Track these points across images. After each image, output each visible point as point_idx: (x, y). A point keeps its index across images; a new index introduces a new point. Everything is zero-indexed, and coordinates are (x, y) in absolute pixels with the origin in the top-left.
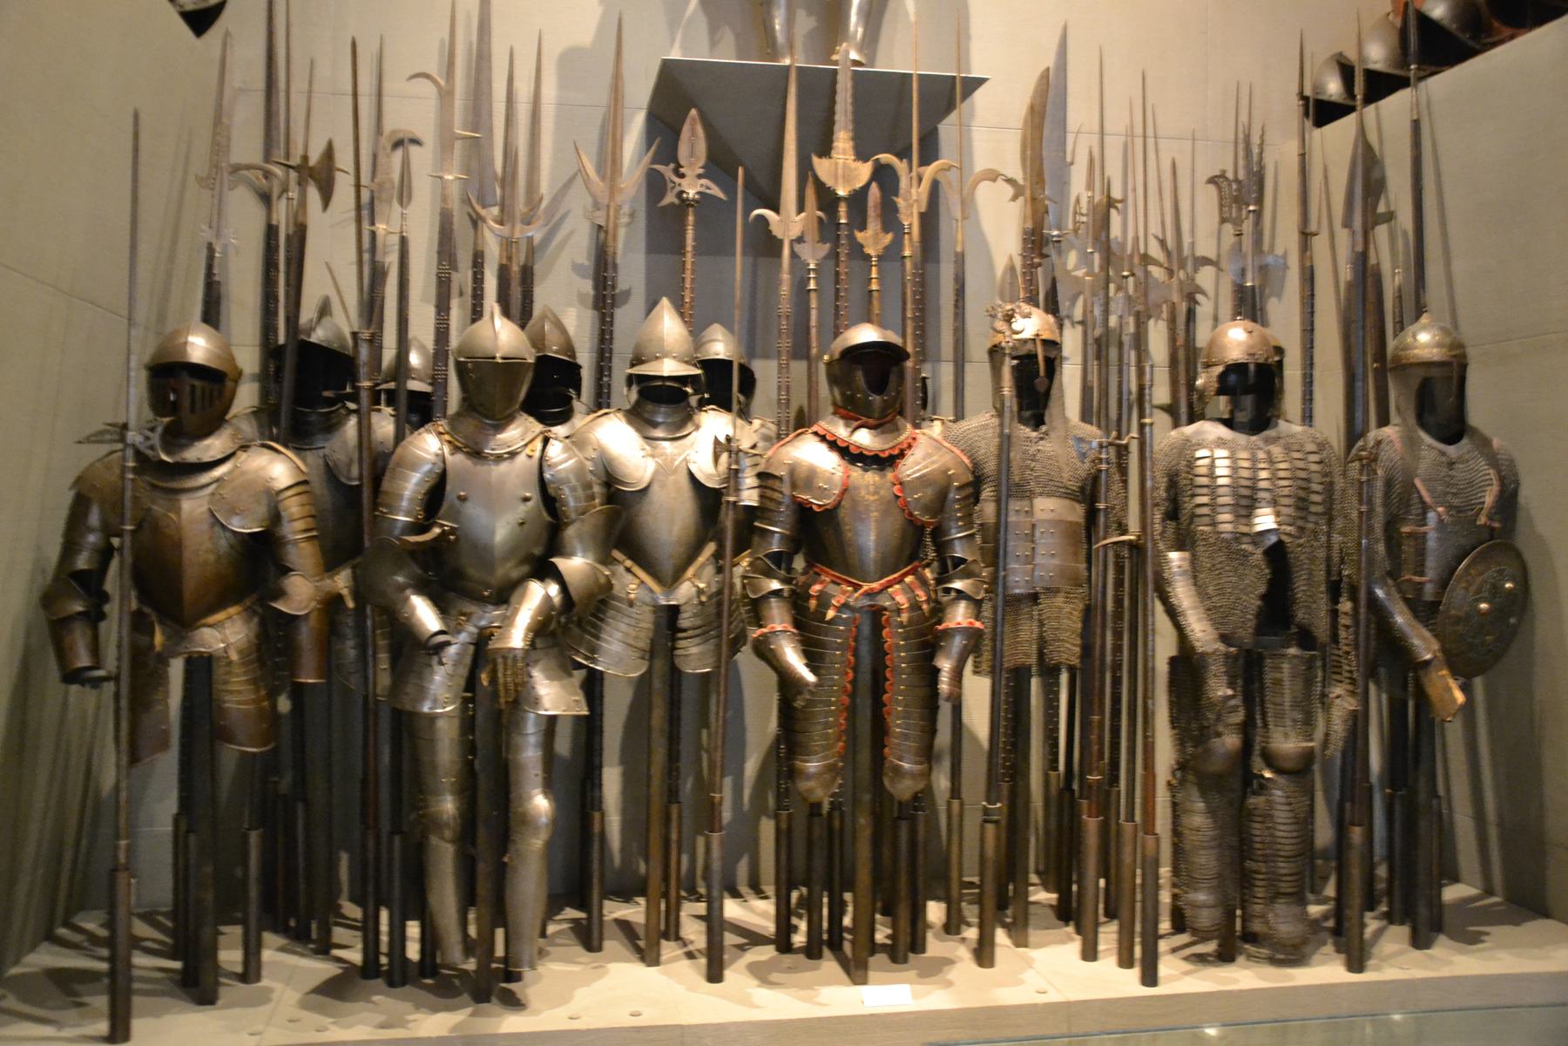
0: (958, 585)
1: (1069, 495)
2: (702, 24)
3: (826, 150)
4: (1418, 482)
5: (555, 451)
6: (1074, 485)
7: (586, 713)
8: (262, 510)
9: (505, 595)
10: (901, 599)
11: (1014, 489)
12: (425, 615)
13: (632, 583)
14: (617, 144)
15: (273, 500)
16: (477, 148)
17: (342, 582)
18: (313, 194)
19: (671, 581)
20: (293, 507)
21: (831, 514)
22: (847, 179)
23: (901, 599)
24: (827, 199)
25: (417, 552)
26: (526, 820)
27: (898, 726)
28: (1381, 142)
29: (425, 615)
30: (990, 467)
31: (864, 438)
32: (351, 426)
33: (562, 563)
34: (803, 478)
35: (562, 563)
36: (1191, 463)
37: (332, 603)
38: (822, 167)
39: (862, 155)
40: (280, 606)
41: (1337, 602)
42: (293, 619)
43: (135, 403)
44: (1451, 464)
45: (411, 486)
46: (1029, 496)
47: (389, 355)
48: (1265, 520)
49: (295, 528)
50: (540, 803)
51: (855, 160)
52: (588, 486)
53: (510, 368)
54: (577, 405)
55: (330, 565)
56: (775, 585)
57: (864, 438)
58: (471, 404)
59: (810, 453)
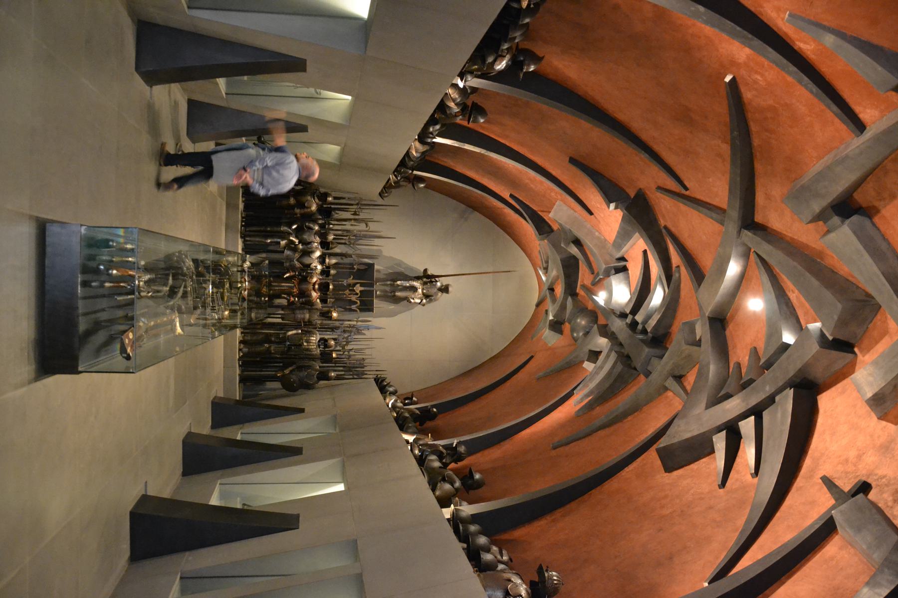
0: (296, 299)
1: (309, 319)
2: (387, 272)
3: (361, 286)
4: (310, 370)
5: (316, 244)
6: (311, 320)
8: (309, 206)
9: (297, 237)
11: (310, 311)
12: (294, 227)
13: (297, 255)
14: (366, 258)
15: (310, 208)
16: (365, 237)
17: (298, 215)
18: (353, 213)
19: (298, 260)
20: (309, 210)
21: (307, 281)
22: (357, 289)
24: (355, 285)
26: (267, 239)
28: (352, 345)
29: (294, 227)
30: (314, 307)
31: (317, 287)
32: (321, 217)
33: (300, 245)
35: (300, 245)
36: (313, 334)
37: (296, 214)
38: (358, 285)
39: (360, 291)
40: (296, 208)
42: (294, 209)
43: (322, 190)
46: (309, 313)
47: (333, 222)
48: (305, 344)
49: (306, 210)
50: (269, 241)
52: (311, 248)
53: (326, 239)
54: (323, 250)
55: (301, 214)
56: (297, 273)
57: (317, 287)
58: (322, 233)
59: (315, 280)
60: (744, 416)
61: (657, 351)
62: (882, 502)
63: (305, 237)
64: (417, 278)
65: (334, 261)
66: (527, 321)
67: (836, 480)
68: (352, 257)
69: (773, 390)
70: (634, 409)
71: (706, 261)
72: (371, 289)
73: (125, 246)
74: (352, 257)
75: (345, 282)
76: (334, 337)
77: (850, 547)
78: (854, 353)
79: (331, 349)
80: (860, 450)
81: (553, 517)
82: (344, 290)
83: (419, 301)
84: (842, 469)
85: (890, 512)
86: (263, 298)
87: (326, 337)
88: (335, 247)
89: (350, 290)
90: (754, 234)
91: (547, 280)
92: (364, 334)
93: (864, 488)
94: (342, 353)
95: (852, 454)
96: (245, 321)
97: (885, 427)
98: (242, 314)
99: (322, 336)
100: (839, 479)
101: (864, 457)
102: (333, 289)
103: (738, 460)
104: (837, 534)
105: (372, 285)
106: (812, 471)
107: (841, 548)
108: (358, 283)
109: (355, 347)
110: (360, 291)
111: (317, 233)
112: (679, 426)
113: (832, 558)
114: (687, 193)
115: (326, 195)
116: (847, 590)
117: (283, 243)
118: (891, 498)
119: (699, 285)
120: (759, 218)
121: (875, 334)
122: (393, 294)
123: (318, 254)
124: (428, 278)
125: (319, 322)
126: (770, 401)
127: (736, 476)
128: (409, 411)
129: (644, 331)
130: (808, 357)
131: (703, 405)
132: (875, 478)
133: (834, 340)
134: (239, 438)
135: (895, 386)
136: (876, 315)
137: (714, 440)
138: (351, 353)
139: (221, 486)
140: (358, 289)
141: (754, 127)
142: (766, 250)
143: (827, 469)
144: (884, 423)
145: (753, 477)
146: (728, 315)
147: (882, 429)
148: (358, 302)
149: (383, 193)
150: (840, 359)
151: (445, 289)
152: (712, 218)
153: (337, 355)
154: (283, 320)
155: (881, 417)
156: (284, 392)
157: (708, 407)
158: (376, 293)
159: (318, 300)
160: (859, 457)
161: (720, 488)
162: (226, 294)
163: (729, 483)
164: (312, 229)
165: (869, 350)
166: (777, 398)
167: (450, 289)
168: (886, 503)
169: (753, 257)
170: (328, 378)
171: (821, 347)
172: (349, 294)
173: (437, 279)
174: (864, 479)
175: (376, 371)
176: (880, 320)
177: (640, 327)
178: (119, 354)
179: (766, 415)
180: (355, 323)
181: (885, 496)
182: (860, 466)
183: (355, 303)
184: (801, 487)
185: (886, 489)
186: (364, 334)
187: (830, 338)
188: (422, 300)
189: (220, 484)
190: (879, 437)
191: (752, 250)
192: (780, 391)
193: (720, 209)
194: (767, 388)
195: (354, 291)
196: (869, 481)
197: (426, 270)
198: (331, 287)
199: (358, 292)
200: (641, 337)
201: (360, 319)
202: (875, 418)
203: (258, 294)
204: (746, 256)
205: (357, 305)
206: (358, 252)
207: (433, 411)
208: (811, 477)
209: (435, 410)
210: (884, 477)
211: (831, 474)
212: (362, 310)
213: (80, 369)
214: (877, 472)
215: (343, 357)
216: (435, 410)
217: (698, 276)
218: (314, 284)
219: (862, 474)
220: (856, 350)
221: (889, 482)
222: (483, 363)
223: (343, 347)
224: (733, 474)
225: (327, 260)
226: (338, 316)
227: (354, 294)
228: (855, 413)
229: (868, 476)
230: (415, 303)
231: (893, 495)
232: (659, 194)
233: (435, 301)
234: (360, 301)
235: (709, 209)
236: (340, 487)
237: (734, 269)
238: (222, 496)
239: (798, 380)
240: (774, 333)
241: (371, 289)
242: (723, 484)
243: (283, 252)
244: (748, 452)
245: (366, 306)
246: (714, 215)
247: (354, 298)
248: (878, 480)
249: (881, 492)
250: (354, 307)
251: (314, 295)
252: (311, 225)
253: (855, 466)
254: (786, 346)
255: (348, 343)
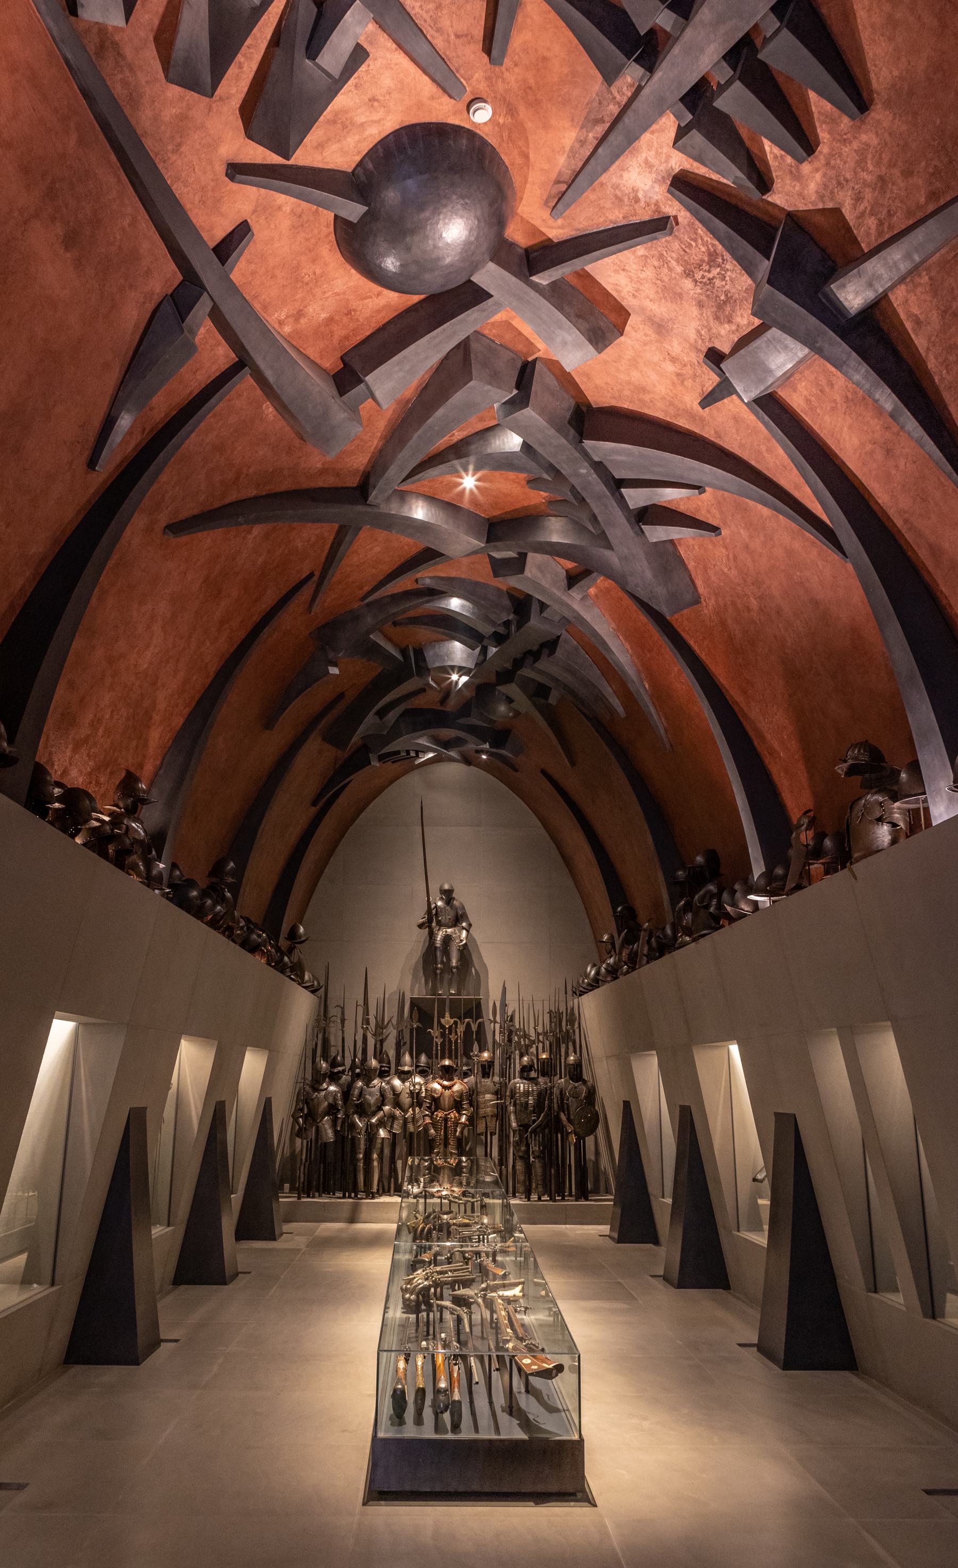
1: (493, 1094)
3: (444, 1017)
5: (383, 1084)
7: (655, 1061)
10: (453, 1116)
21: (439, 1098)
23: (453, 1116)
24: (443, 1027)
25: (357, 1105)
27: (413, 1161)
31: (446, 1083)
34: (434, 1090)
38: (442, 1021)
39: (451, 1018)
41: (424, 1261)
44: (576, 1088)
45: (356, 1092)
51: (285, 938)
57: (446, 1083)
59: (436, 1086)
60: (622, 501)
61: (535, 608)
62: (731, 336)
63: (372, 1099)
64: (432, 935)
65: (407, 1058)
66: (491, 777)
67: (705, 389)
68: (402, 1030)
69: (586, 464)
70: (629, 1112)
71: (408, 545)
72: (448, 1002)
73: (402, 1370)
74: (402, 1030)
75: (437, 1040)
76: (517, 1057)
77: (792, 379)
78: (535, 360)
79: (535, 1061)
80: (665, 358)
81: (766, 753)
82: (450, 1041)
83: (464, 933)
84: (690, 380)
85: (744, 328)
86: (464, 1164)
87: (518, 1068)
88: (387, 1056)
89: (450, 1033)
90: (374, 487)
91: (433, 750)
92: (514, 1011)
93: (715, 357)
94: (541, 1045)
95: (670, 368)
96: (497, 1192)
97: (633, 328)
98: (486, 1195)
99: (517, 1074)
100: (703, 386)
101: (674, 354)
102: (450, 1058)
103: (682, 508)
104: (776, 393)
105: (442, 1002)
106: (692, 417)
107: (795, 390)
108: (439, 1022)
109: (532, 1025)
110: (451, 1018)
111: (368, 1082)
112: (637, 585)
113: (808, 401)
114: (317, 574)
115: (316, 1070)
116: (847, 386)
117: (382, 1133)
118: (726, 326)
119: (443, 555)
120: (353, 482)
121: (508, 336)
122: (454, 970)
123: (397, 1082)
124: (431, 919)
125: (496, 1079)
126: (599, 467)
127: (703, 512)
128: (622, 947)
129: (507, 624)
130: (541, 421)
131: (607, 553)
132: (700, 342)
133: (517, 387)
134: (669, 1201)
135: (579, 316)
136: (483, 335)
137: (655, 540)
138: (540, 1030)
139: (741, 1228)
140: (448, 1020)
141: (232, 497)
142: (394, 473)
143: (691, 400)
144: (627, 328)
145: (704, 491)
146: (483, 515)
147: (636, 332)
148: (467, 1020)
149: (312, 986)
150: (542, 381)
151: (448, 895)
152: (351, 543)
153: (544, 1051)
154: (495, 1134)
155: (619, 332)
156: (600, 1131)
157: (609, 547)
158: (452, 994)
159: (466, 1080)
160: (674, 360)
161: (720, 534)
162: (460, 1220)
163: (714, 523)
164: (362, 1089)
165: (530, 344)
166: (597, 459)
167: (446, 887)
168: (733, 332)
169: (404, 487)
170: (578, 1066)
171: (527, 406)
172: (456, 1034)
173: (433, 906)
174: (702, 356)
175: (566, 993)
176: (490, 330)
177: (501, 630)
178: (553, 1380)
179: (618, 475)
180: (498, 1026)
181: (723, 332)
182: (685, 358)
183: (468, 1025)
184: (716, 432)
185: (714, 331)
186: (514, 1011)
187: (515, 392)
188: (463, 928)
189: (738, 1231)
190: (646, 335)
191: (396, 488)
192: (585, 454)
193: (339, 532)
194: (583, 471)
195: (450, 1027)
196: (705, 350)
197: (421, 926)
198: (447, 1062)
199: (452, 1021)
200: (513, 628)
201: (491, 1018)
202: (622, 338)
203: (457, 1171)
204: (403, 496)
205: (471, 1023)
206: (394, 1021)
207: (620, 912)
208: (702, 419)
209: (619, 909)
210: (698, 332)
211: (698, 394)
212: (479, 1015)
213: (576, 1437)
214: (692, 341)
215: (547, 1043)
216: (619, 909)
217: (429, 555)
218: (444, 1087)
219: (696, 358)
220: (530, 359)
221: (706, 327)
222: (552, 838)
223: (533, 1042)
224: (701, 516)
225: (406, 1068)
226: (488, 1050)
227: (456, 1027)
228: (615, 362)
229: (698, 350)
230: (467, 937)
231: (721, 323)
232: (316, 609)
233: (464, 908)
234: (464, 1019)
235: (339, 545)
236: (734, 1049)
237: (420, 512)
238: (756, 1226)
239: (572, 432)
240: (505, 462)
241: (448, 1002)
242: (715, 529)
243: (394, 1134)
244: (669, 495)
245: (474, 1010)
246: (348, 538)
247: (461, 1029)
248: (703, 340)
249: (718, 336)
250: (474, 1028)
251: (457, 1088)
252: (356, 1092)
253: (685, 365)
254: (526, 447)
255: (526, 1036)
